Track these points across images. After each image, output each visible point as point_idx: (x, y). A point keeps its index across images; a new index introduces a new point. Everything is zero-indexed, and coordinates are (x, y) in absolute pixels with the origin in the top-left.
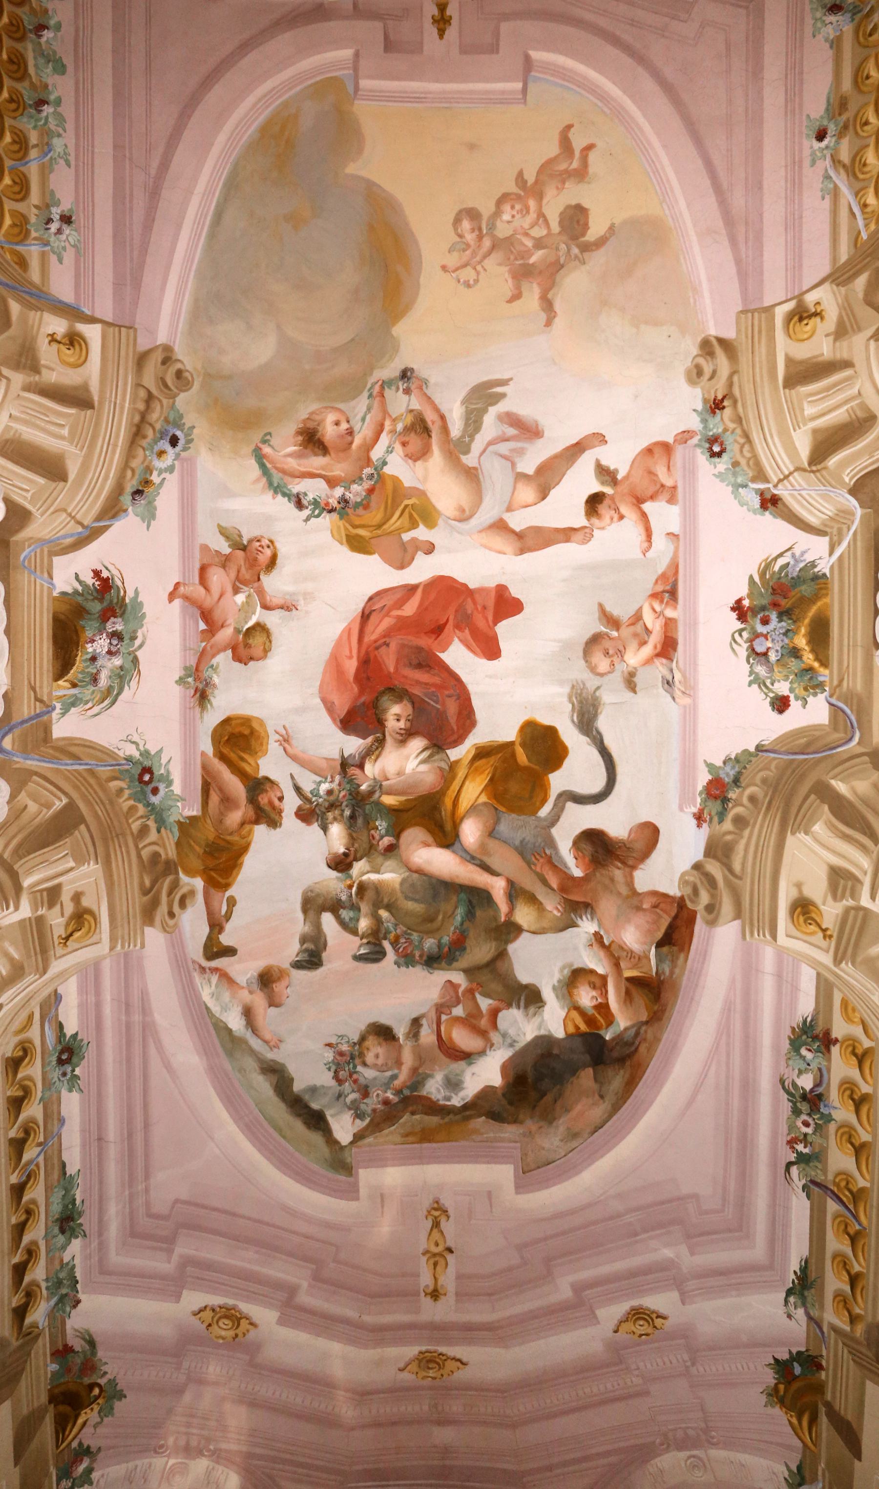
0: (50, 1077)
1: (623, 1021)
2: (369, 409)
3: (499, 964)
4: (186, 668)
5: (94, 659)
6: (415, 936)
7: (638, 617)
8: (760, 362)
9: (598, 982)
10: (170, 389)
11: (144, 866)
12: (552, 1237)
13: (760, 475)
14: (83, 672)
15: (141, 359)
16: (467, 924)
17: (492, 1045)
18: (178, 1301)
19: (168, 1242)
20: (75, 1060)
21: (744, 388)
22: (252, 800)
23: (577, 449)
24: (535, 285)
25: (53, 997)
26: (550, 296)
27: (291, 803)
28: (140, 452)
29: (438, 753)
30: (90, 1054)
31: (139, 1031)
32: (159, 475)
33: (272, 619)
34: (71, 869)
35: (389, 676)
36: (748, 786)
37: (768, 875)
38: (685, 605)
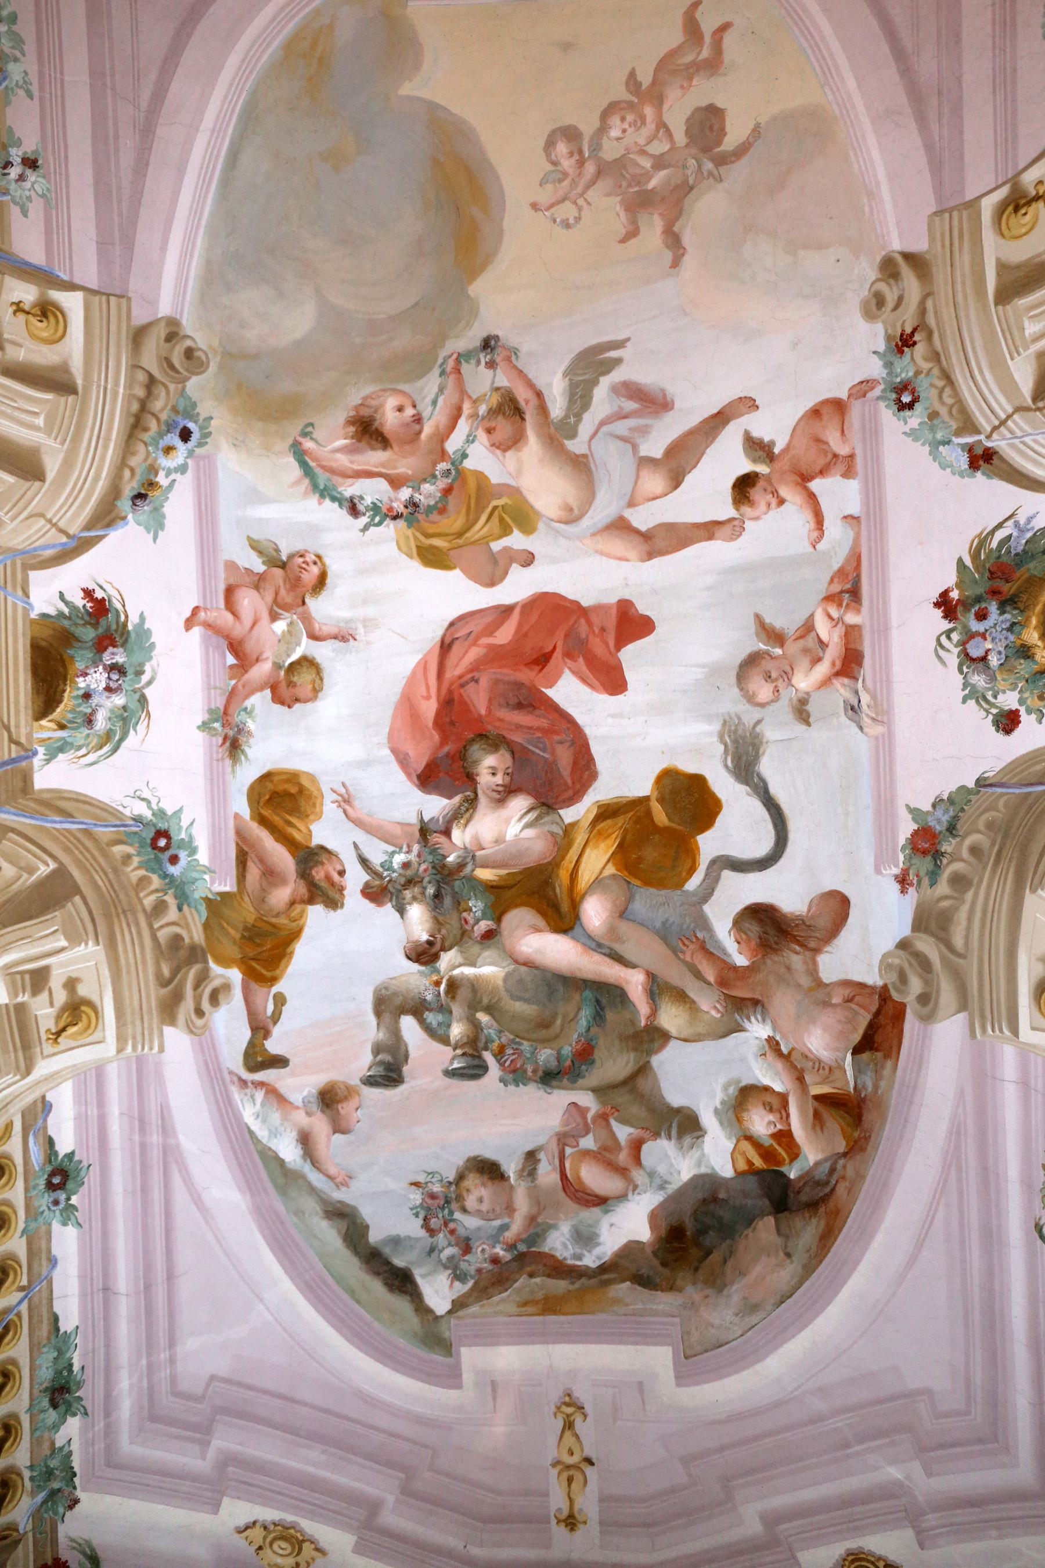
0: (36, 1204)
1: (812, 1153)
2: (441, 390)
3: (640, 1081)
4: (210, 711)
5: (87, 696)
6: (526, 1046)
7: (808, 627)
8: (963, 275)
9: (776, 1103)
10: (178, 372)
11: (161, 952)
12: (733, 1445)
13: (968, 425)
14: (73, 711)
15: (138, 336)
16: (594, 1030)
17: (635, 1187)
18: (216, 1513)
19: (200, 1432)
20: (70, 1185)
21: (942, 315)
22: (304, 874)
23: (720, 419)
24: (656, 218)
25: (39, 1105)
26: (676, 229)
27: (355, 878)
28: (141, 448)
29: (548, 813)
30: (92, 1179)
31: (158, 1157)
32: (167, 476)
33: (323, 652)
34: (62, 950)
35: (479, 719)
36: (968, 834)
37: (1002, 950)
38: (871, 607)
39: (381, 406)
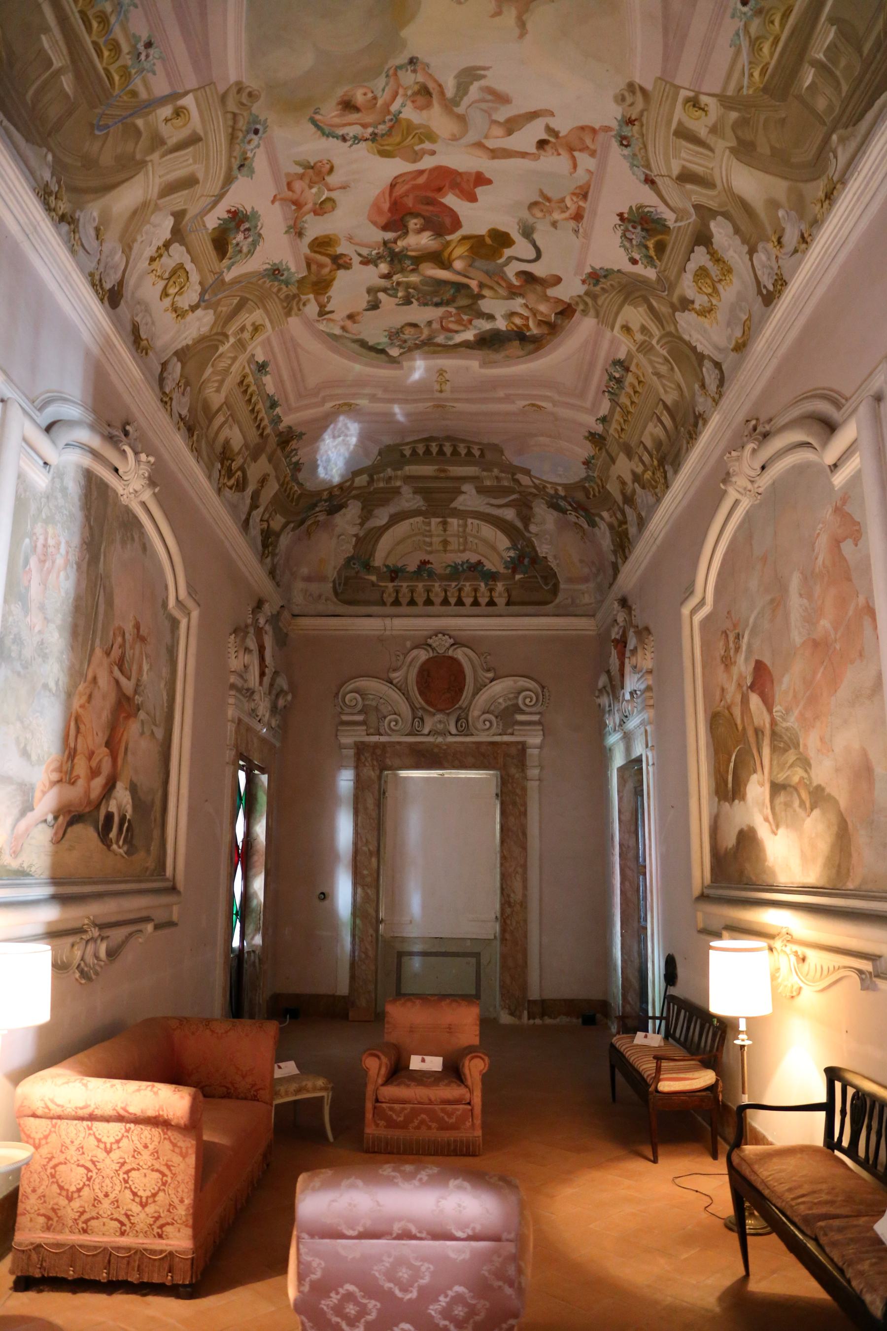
2: (387, 84)
5: (238, 244)
7: (563, 200)
13: (648, 166)
15: (223, 98)
23: (534, 115)
26: (524, 18)
33: (334, 195)
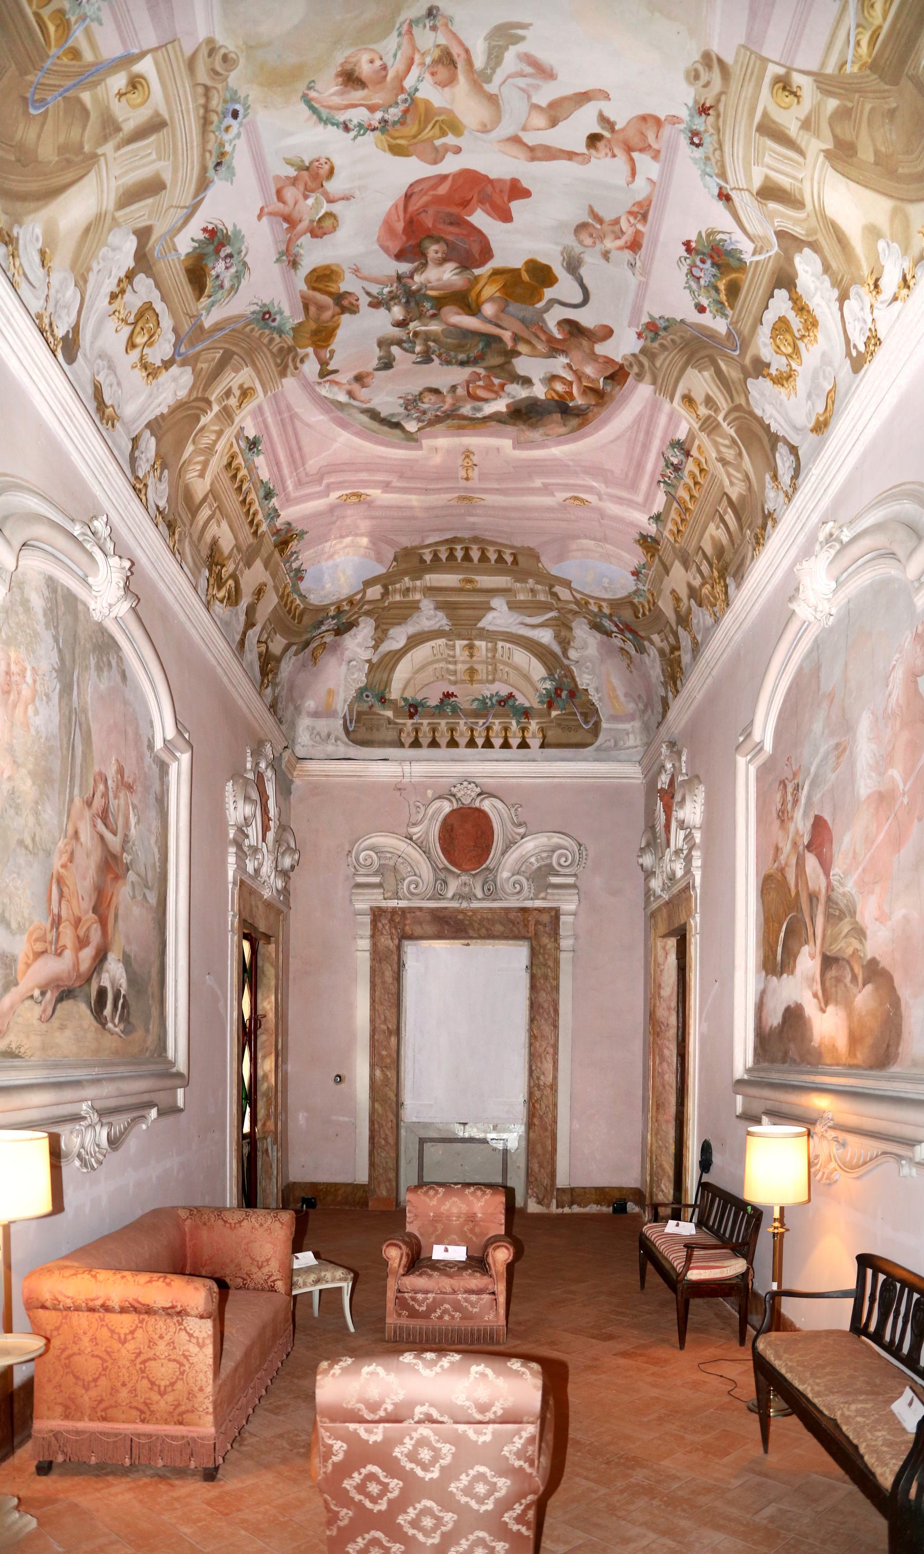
2: (399, 47)
3: (506, 366)
5: (218, 277)
6: (452, 353)
7: (617, 222)
13: (723, 175)
23: (584, 97)
28: (212, 136)
33: (336, 208)
35: (429, 229)
39: (359, 61)
